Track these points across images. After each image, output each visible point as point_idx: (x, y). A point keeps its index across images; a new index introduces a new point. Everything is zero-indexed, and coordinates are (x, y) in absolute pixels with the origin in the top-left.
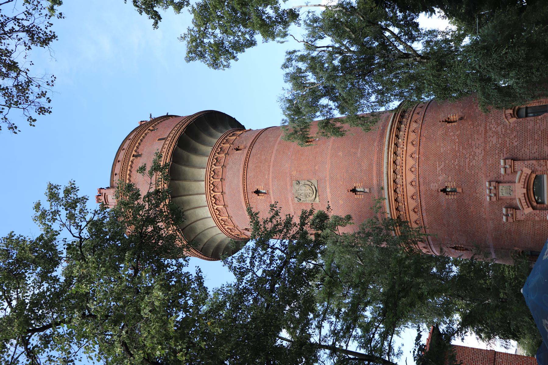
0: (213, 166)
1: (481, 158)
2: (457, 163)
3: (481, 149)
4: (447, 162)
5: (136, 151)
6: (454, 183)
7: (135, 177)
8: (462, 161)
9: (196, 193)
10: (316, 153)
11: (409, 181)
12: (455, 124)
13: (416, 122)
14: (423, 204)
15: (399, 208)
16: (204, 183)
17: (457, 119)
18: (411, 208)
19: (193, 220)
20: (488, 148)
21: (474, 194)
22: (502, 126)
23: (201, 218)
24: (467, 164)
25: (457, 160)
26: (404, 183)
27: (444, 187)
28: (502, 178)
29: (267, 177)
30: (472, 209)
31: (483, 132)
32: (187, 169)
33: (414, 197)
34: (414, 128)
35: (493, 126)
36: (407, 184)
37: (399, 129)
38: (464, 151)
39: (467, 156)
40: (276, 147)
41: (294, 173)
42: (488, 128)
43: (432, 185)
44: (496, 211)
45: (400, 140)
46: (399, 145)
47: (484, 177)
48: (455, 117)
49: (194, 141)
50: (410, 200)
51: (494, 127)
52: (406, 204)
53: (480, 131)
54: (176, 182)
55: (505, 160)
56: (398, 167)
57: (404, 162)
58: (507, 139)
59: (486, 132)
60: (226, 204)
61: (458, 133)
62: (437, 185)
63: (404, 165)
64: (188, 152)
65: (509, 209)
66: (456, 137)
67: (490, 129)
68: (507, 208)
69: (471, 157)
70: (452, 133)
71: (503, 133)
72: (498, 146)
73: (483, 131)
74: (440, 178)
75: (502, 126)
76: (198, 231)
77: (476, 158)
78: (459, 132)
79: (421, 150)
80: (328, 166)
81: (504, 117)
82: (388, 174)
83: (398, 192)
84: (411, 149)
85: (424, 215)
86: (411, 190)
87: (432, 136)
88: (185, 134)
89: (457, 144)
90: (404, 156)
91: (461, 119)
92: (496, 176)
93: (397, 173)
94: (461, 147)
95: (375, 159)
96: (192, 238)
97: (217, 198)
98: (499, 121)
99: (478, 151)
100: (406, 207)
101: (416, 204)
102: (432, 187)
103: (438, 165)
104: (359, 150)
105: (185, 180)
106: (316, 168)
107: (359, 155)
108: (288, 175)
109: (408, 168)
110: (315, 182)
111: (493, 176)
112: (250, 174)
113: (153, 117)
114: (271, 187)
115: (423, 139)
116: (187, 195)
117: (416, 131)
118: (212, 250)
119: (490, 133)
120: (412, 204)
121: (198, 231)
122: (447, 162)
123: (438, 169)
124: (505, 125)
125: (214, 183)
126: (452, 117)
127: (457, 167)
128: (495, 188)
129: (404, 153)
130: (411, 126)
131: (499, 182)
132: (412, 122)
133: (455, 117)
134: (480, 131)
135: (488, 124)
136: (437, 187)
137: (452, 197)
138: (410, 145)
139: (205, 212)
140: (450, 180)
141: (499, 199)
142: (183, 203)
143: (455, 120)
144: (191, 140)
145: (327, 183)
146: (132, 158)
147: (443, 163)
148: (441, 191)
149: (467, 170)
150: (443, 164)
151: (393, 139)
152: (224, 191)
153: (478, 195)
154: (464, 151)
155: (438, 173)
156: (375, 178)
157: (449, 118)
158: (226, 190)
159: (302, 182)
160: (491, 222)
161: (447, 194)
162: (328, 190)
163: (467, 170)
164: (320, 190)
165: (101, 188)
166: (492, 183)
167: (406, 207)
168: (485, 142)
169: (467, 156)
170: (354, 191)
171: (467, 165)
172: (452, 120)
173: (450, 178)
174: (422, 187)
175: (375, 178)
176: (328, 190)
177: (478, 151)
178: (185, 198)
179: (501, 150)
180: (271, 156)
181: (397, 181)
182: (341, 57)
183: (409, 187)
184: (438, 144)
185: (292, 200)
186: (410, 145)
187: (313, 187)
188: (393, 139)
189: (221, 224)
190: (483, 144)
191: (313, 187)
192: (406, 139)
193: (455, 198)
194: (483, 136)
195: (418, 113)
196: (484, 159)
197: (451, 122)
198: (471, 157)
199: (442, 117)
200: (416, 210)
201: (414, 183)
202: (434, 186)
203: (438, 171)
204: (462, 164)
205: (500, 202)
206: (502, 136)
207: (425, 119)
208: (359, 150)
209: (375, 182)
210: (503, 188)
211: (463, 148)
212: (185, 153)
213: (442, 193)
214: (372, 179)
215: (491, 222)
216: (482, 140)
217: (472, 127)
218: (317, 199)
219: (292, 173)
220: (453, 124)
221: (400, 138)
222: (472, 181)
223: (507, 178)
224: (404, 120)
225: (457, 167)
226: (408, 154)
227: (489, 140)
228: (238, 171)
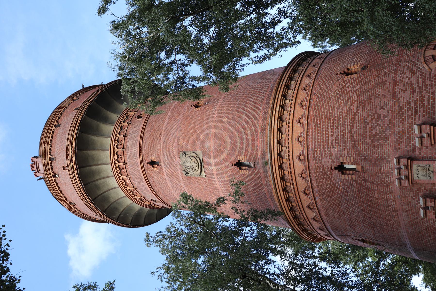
0: (118, 135)
1: (387, 122)
2: (354, 130)
3: (387, 109)
4: (342, 128)
5: (57, 122)
6: (352, 158)
7: (54, 147)
8: (362, 127)
9: (104, 162)
10: (203, 119)
11: (296, 154)
12: (355, 76)
13: (309, 76)
14: (315, 184)
15: (288, 189)
16: (109, 152)
17: (360, 69)
18: (301, 189)
19: (105, 189)
20: (397, 107)
21: (379, 175)
22: (419, 74)
23: (112, 187)
24: (368, 131)
25: (355, 126)
26: (291, 157)
27: (339, 164)
28: (417, 152)
29: (158, 147)
30: (376, 196)
31: (391, 86)
32: (95, 138)
33: (304, 175)
34: (305, 85)
35: (405, 76)
36: (295, 158)
37: (288, 87)
38: (365, 114)
39: (369, 119)
40: (169, 114)
41: (181, 143)
42: (398, 78)
43: (323, 160)
44: (411, 200)
45: (287, 101)
46: (286, 107)
47: (391, 151)
48: (356, 67)
49: (104, 110)
50: (299, 179)
51: (406, 77)
52: (295, 184)
53: (388, 83)
54: (84, 152)
55: (420, 126)
56: (284, 136)
57: (290, 129)
58: (426, 94)
59: (395, 84)
60: (129, 174)
61: (357, 88)
62: (330, 161)
63: (290, 133)
64: (98, 121)
65: (428, 200)
66: (355, 94)
67: (402, 80)
68: (425, 197)
69: (374, 121)
70: (350, 89)
71: (420, 84)
72: (412, 104)
73: (392, 83)
74: (334, 151)
75: (419, 74)
76: (112, 200)
77: (380, 123)
78: (359, 86)
79: (311, 114)
80: (212, 135)
81: (422, 61)
82: (270, 146)
83: (285, 168)
84: (300, 112)
85: (317, 198)
86: (299, 167)
87: (325, 93)
88: (95, 103)
89: (356, 103)
90: (291, 121)
91: (364, 68)
92: (408, 148)
93: (283, 143)
94: (361, 108)
95: (260, 126)
96: (106, 207)
97: (121, 168)
98: (414, 68)
99: (383, 112)
100: (295, 187)
101: (306, 184)
102: (323, 164)
103: (330, 134)
104: (244, 115)
105: (94, 149)
106: (201, 137)
107: (243, 121)
108: (176, 145)
109: (295, 137)
110: (199, 153)
111: (404, 149)
112: (145, 144)
113: (85, 87)
114: (162, 158)
115: (314, 98)
116: (96, 165)
117: (307, 88)
118: (131, 218)
119: (401, 86)
120: (302, 184)
121: (112, 200)
122: (342, 128)
123: (331, 138)
124: (423, 74)
125: (118, 153)
126: (352, 68)
127: (355, 136)
128: (406, 167)
129: (291, 117)
130: (303, 82)
131: (412, 159)
132: (304, 77)
133: (356, 67)
134: (388, 83)
135: (399, 73)
136: (330, 164)
137: (350, 178)
138: (298, 107)
139: (113, 182)
140: (346, 155)
141: (413, 183)
142: (93, 173)
143: (356, 70)
144: (103, 109)
145: (212, 155)
146: (53, 128)
147: (337, 130)
148: (336, 168)
149: (368, 141)
150: (337, 132)
151: (279, 100)
152: (126, 161)
153: (384, 176)
154: (365, 114)
155: (330, 144)
156: (259, 150)
157: (348, 69)
158: (128, 160)
159: (188, 154)
160: (404, 214)
161: (343, 173)
162: (213, 163)
163: (368, 141)
164: (205, 163)
165: (35, 157)
166: (401, 160)
167: (295, 187)
168: (394, 100)
169: (368, 121)
170: (239, 164)
171: (368, 134)
172: (353, 71)
173: (346, 150)
174: (312, 163)
175: (259, 150)
176: (213, 163)
177: (383, 112)
178: (94, 168)
179: (416, 111)
180: (163, 125)
181: (283, 153)
182: (236, 7)
183: (297, 162)
184: (332, 104)
185: (182, 174)
186: (298, 107)
187: (198, 159)
188: (279, 100)
189: (131, 194)
190: (390, 103)
191: (198, 159)
192: (294, 99)
193: (354, 179)
194: (391, 91)
195: (314, 66)
196: (392, 124)
197: (352, 74)
198: (374, 121)
199: (340, 68)
200: (307, 192)
201: (302, 158)
202: (327, 162)
203: (330, 141)
204: (362, 132)
205: (415, 188)
206: (417, 90)
207: (319, 73)
208: (244, 115)
209: (259, 155)
210: (419, 168)
211: (363, 110)
212: (94, 122)
213: (337, 171)
214: (256, 151)
215: (404, 214)
216: (389, 96)
217: (377, 79)
218: (203, 173)
219: (180, 143)
220: (353, 76)
221: (288, 98)
222: (375, 156)
223: (425, 152)
224: (296, 75)
225: (355, 136)
226: (296, 119)
227: (399, 96)
228: (136, 139)
